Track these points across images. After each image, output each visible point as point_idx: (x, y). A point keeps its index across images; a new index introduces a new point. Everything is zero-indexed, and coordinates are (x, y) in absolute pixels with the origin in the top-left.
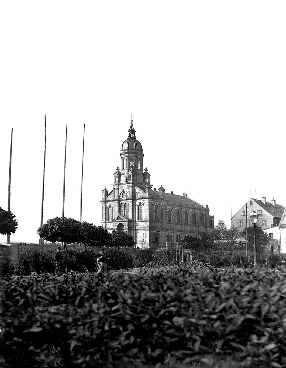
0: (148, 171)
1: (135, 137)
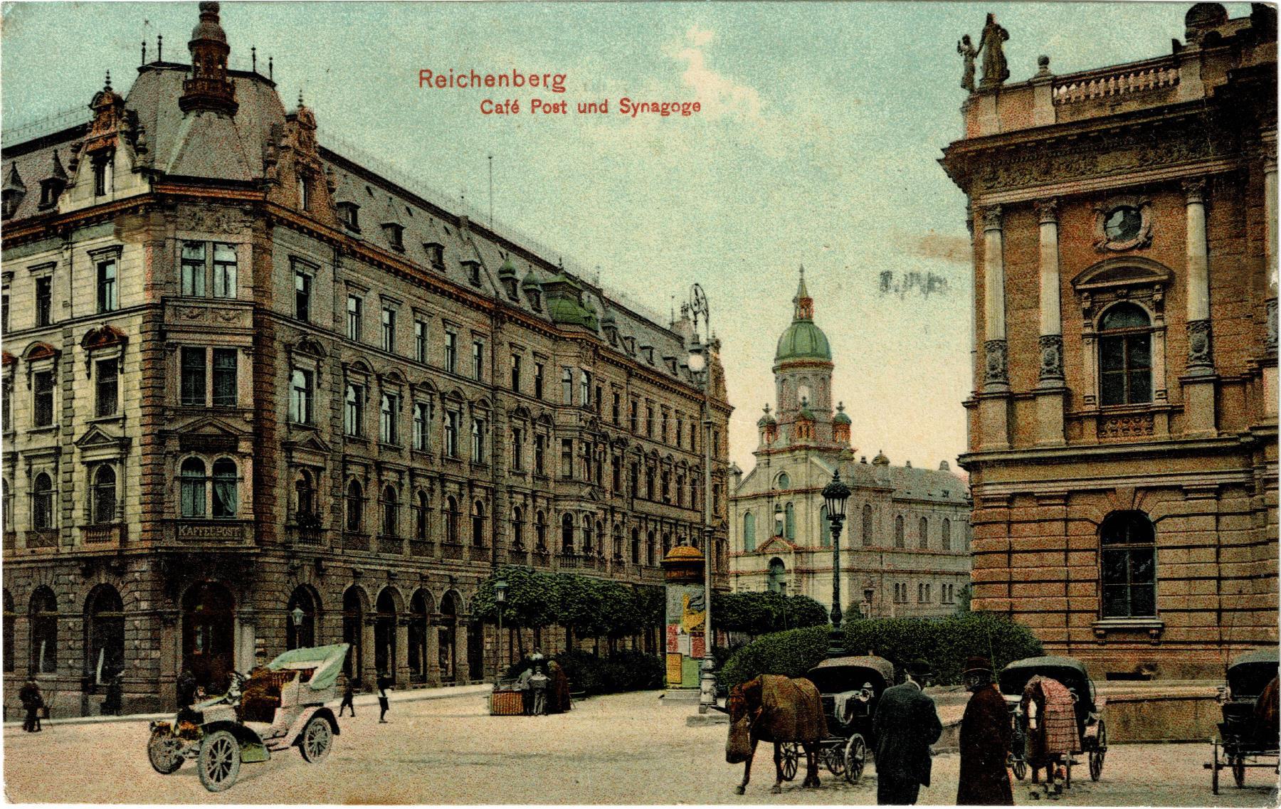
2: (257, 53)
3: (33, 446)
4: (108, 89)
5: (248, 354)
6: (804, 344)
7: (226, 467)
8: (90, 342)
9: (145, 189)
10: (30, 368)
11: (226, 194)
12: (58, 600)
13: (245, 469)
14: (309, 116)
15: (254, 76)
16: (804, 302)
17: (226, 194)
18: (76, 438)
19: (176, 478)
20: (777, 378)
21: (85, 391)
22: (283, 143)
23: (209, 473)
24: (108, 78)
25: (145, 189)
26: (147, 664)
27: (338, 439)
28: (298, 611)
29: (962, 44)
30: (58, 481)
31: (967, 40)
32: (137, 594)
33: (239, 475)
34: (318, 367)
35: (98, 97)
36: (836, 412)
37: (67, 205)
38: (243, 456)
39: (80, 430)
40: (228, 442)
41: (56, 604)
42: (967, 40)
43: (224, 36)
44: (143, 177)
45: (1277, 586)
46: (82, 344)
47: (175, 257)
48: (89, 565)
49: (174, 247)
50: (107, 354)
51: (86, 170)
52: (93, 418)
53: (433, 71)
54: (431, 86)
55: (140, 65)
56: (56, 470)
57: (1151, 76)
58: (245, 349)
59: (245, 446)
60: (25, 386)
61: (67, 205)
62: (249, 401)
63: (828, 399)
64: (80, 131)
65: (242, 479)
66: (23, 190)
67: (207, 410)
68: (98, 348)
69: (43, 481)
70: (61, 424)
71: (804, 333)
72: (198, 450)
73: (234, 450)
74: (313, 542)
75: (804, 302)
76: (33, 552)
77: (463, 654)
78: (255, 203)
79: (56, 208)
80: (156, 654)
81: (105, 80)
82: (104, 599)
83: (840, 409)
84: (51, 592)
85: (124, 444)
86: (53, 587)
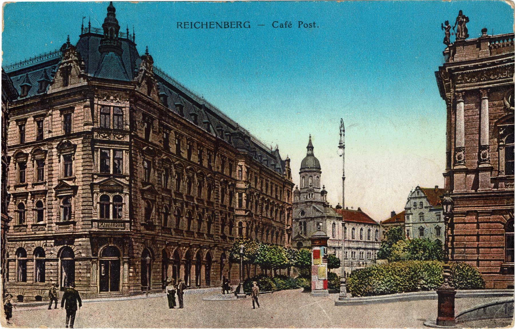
2: (129, 31)
3: (35, 190)
4: (68, 43)
5: (127, 153)
6: (311, 163)
7: (118, 199)
8: (61, 147)
9: (86, 83)
10: (34, 158)
11: (117, 86)
12: (46, 253)
13: (126, 200)
14: (151, 58)
15: (127, 40)
16: (310, 147)
17: (117, 86)
18: (54, 186)
19: (98, 203)
20: (301, 176)
21: (58, 167)
22: (140, 69)
23: (111, 201)
24: (68, 38)
25: (86, 83)
26: (85, 279)
27: (160, 189)
28: (148, 258)
29: (444, 24)
30: (45, 205)
31: (447, 23)
32: (81, 251)
33: (123, 202)
34: (153, 160)
35: (64, 46)
36: (322, 189)
37: (51, 90)
38: (126, 194)
39: (55, 183)
40: (120, 187)
41: (45, 255)
42: (447, 23)
43: (117, 22)
44: (84, 79)
45: (111, 327)
46: (57, 148)
47: (98, 112)
48: (58, 239)
49: (97, 108)
50: (67, 152)
51: (59, 77)
52: (62, 178)
53: (242, 22)
54: (241, 27)
55: (80, 34)
56: (45, 200)
57: (506, 41)
58: (126, 150)
59: (126, 191)
60: (31, 165)
61: (51, 90)
62: (128, 172)
63: (318, 184)
64: (56, 61)
65: (125, 204)
66: (30, 85)
67: (111, 175)
68: (64, 150)
69: (40, 204)
70: (47, 181)
71: (310, 159)
72: (107, 191)
73: (121, 192)
74: (152, 230)
75: (310, 147)
76: (35, 233)
77: (203, 277)
78: (130, 90)
79: (45, 92)
80: (89, 275)
81: (67, 39)
82: (67, 252)
83: (324, 188)
84: (43, 249)
85: (75, 189)
86: (43, 247)
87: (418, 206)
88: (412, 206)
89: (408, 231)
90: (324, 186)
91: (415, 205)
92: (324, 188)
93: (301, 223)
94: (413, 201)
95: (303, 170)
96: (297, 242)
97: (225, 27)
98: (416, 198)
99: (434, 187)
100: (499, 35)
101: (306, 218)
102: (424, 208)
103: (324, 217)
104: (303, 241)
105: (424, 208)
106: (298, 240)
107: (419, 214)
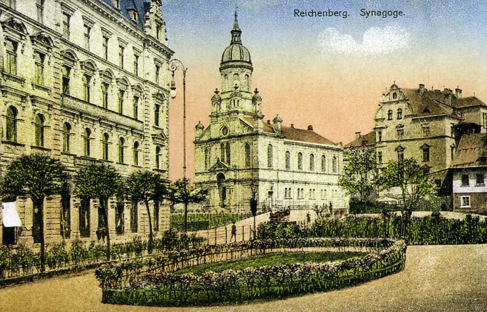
0: (259, 93)
1: (240, 40)
71: (236, 48)
87: (395, 115)
88: (386, 117)
89: (380, 153)
90: (256, 89)
91: (390, 113)
92: (256, 92)
93: (222, 145)
94: (386, 108)
95: (223, 65)
96: (218, 173)
97: (329, 16)
98: (390, 103)
99: (418, 87)
100: (124, 152)
101: (230, 137)
102: (322, 12)
103: (201, 251)
104: (226, 171)
105: (322, 12)
106: (218, 171)
107: (396, 127)
